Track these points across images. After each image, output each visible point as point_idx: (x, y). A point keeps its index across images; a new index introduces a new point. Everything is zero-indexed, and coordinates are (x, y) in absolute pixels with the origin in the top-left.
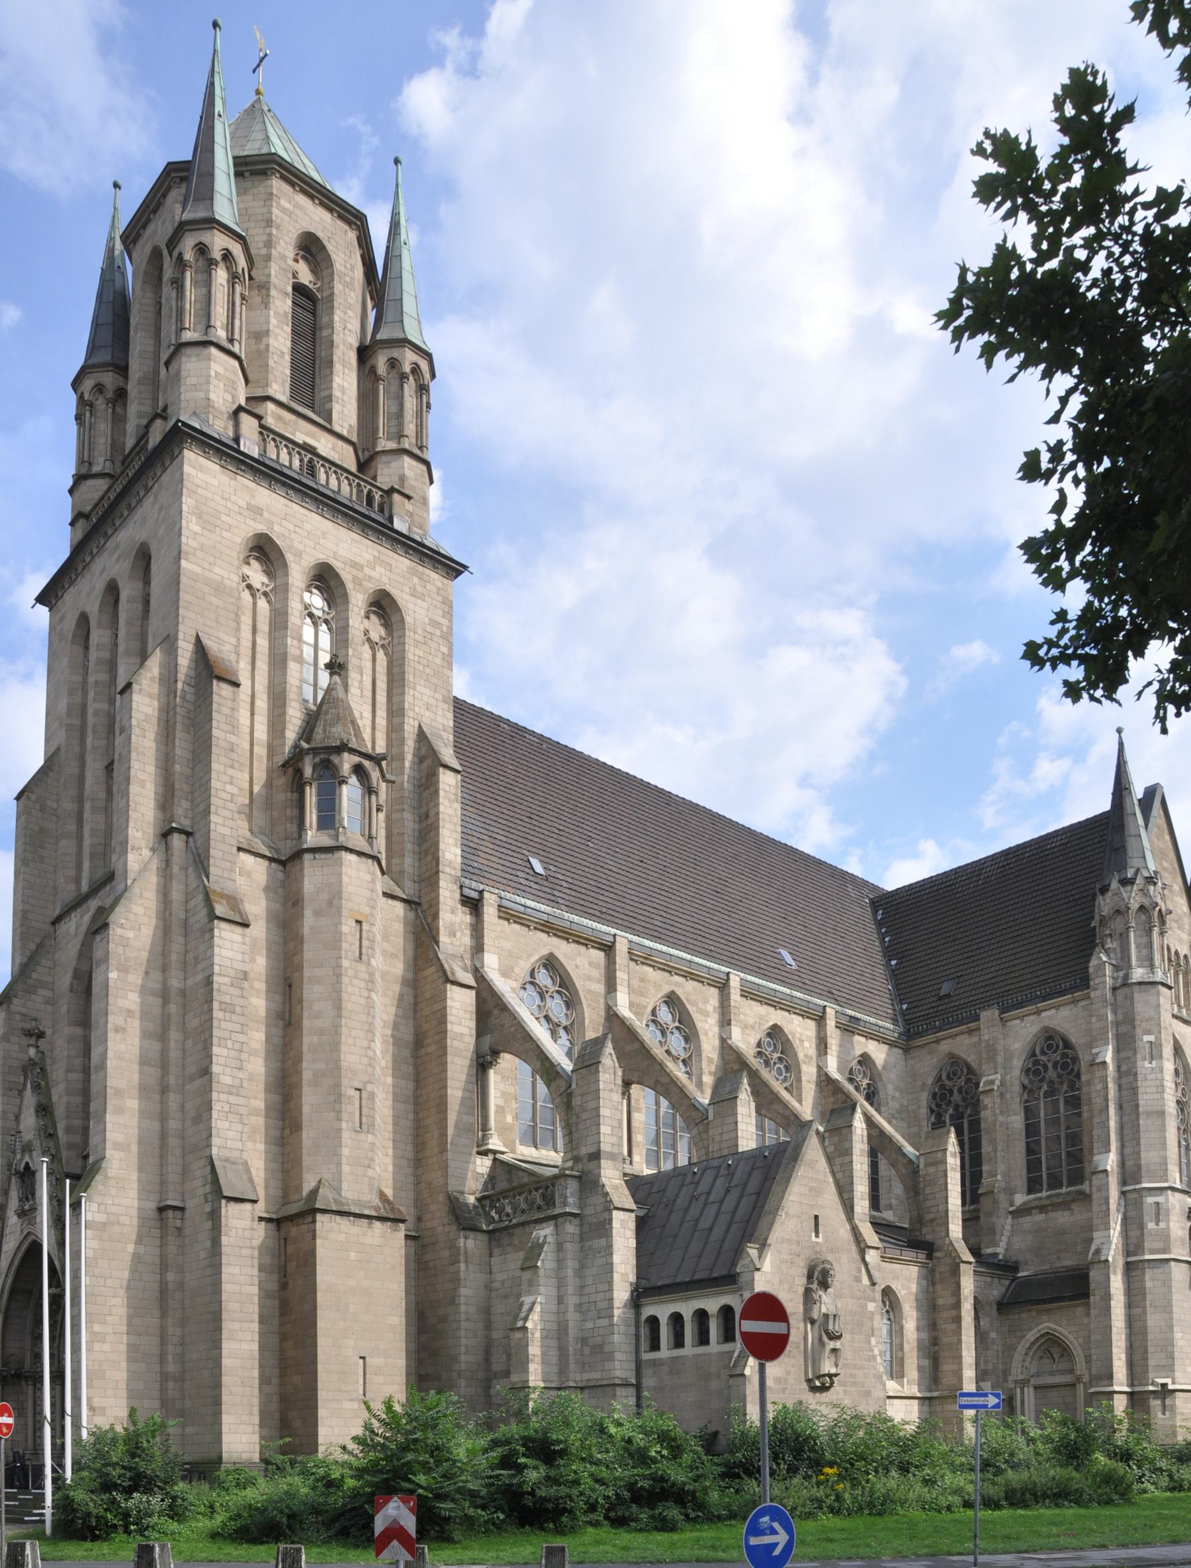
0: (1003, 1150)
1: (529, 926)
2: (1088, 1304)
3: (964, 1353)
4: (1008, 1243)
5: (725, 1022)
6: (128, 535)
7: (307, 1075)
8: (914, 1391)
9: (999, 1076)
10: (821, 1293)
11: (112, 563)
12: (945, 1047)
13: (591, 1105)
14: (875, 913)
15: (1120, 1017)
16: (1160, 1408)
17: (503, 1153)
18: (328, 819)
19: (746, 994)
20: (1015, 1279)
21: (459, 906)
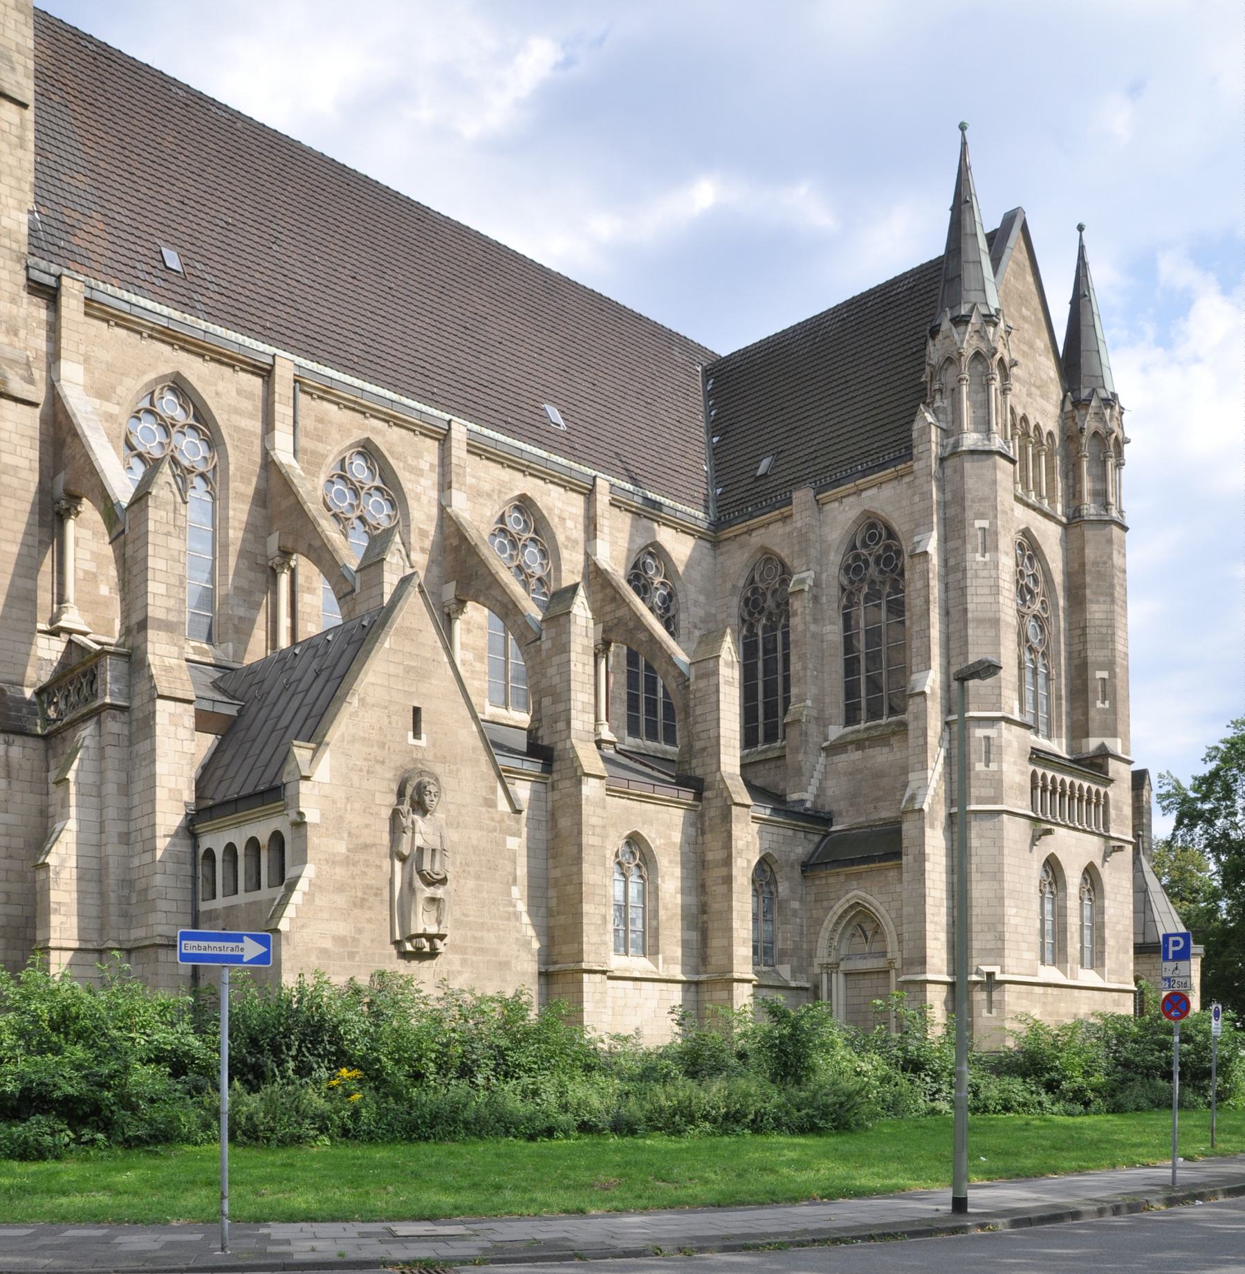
0: (815, 669)
1: (141, 333)
2: (900, 867)
3: (736, 924)
5: (445, 485)
8: (677, 972)
9: (812, 573)
10: (416, 817)
12: (757, 539)
14: (705, 383)
15: (949, 496)
16: (985, 1003)
17: (85, 634)
19: (474, 449)
20: (827, 834)
21: (24, 294)
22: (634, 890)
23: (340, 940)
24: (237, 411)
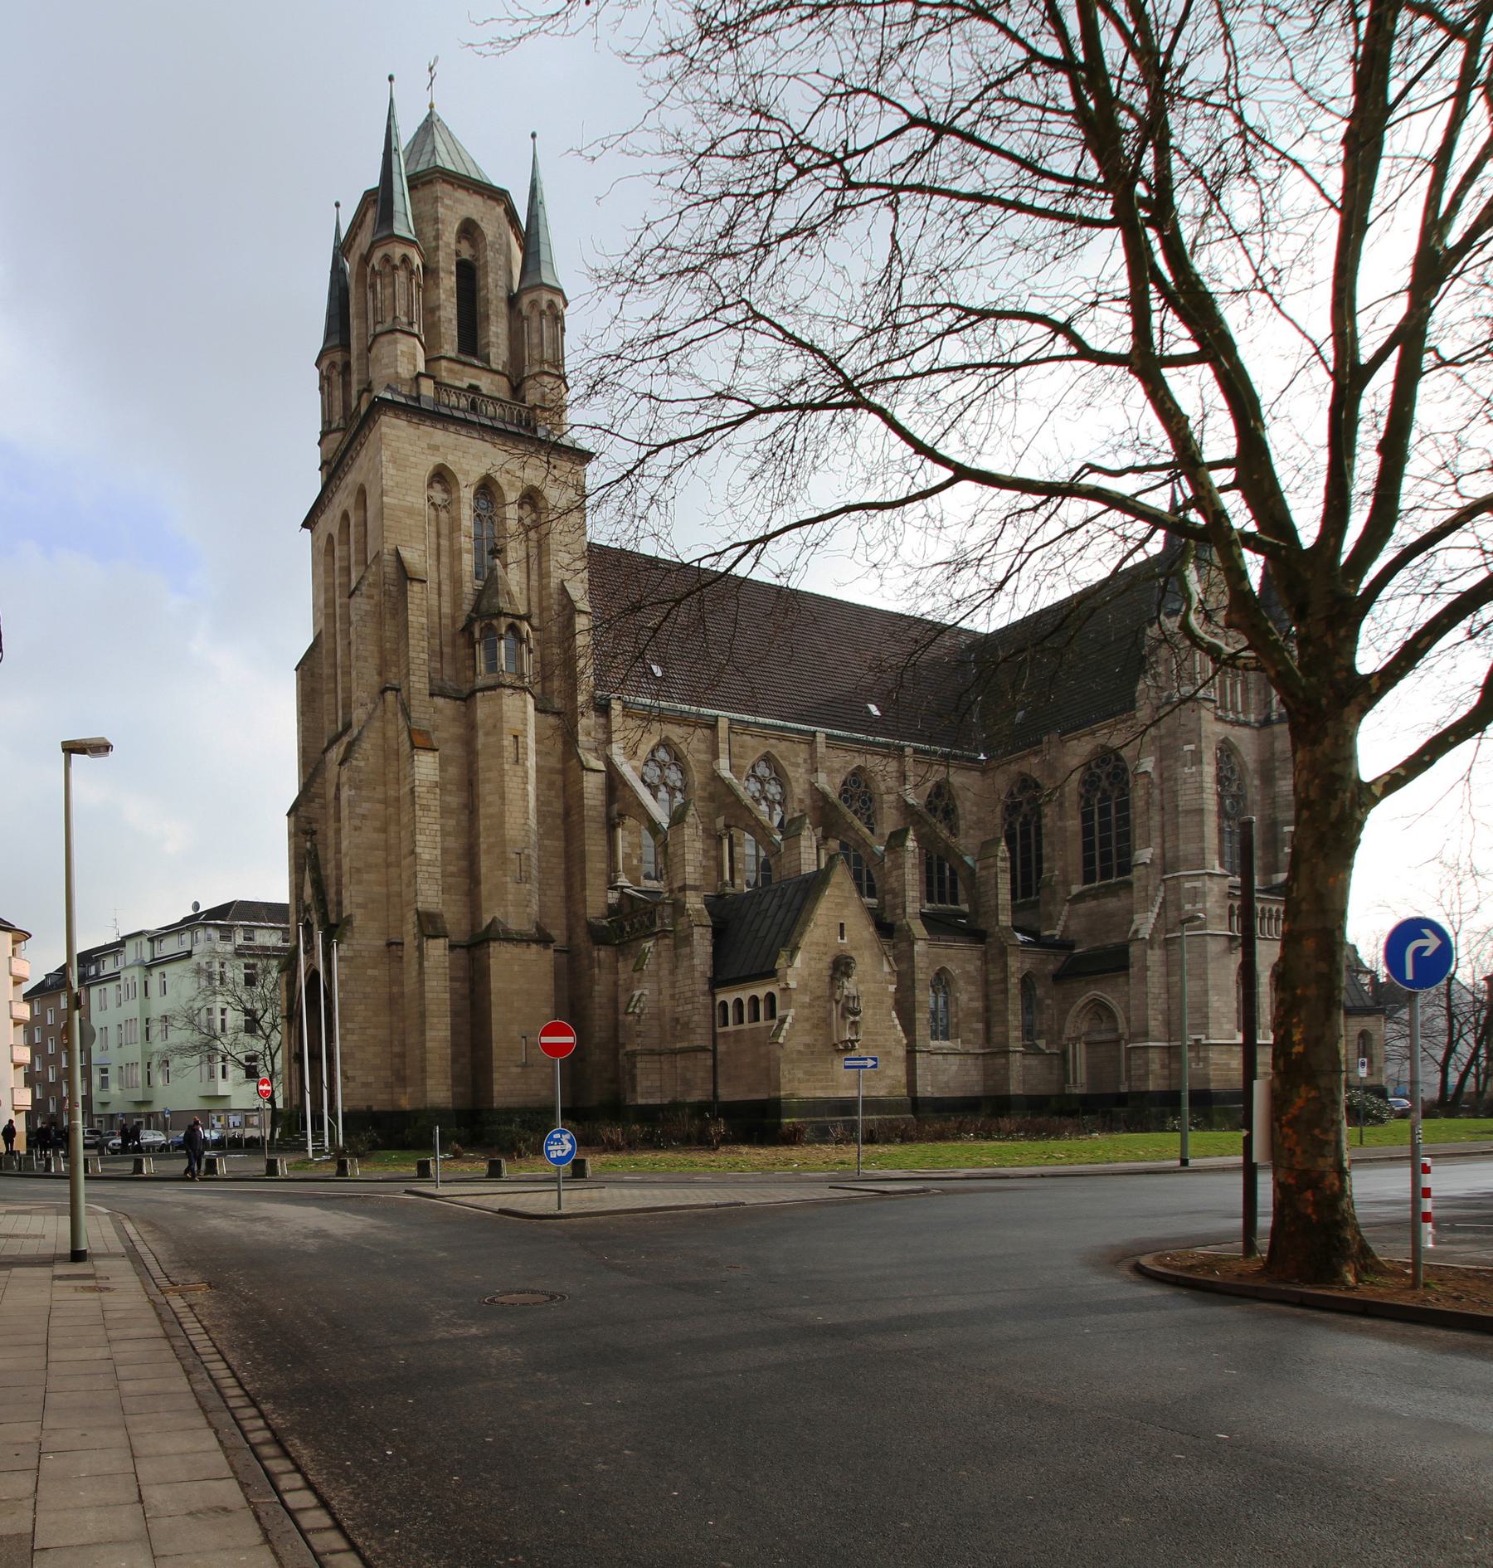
4: (1066, 927)
6: (352, 478)
7: (483, 847)
11: (344, 500)
13: (680, 852)
18: (492, 665)
22: (941, 1002)
23: (807, 1046)
24: (698, 751)
